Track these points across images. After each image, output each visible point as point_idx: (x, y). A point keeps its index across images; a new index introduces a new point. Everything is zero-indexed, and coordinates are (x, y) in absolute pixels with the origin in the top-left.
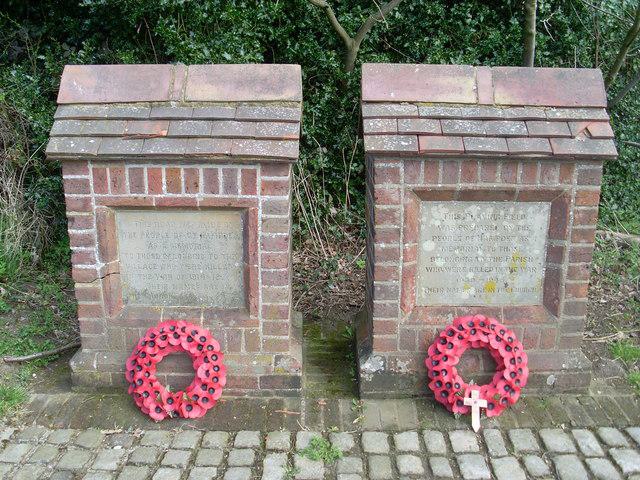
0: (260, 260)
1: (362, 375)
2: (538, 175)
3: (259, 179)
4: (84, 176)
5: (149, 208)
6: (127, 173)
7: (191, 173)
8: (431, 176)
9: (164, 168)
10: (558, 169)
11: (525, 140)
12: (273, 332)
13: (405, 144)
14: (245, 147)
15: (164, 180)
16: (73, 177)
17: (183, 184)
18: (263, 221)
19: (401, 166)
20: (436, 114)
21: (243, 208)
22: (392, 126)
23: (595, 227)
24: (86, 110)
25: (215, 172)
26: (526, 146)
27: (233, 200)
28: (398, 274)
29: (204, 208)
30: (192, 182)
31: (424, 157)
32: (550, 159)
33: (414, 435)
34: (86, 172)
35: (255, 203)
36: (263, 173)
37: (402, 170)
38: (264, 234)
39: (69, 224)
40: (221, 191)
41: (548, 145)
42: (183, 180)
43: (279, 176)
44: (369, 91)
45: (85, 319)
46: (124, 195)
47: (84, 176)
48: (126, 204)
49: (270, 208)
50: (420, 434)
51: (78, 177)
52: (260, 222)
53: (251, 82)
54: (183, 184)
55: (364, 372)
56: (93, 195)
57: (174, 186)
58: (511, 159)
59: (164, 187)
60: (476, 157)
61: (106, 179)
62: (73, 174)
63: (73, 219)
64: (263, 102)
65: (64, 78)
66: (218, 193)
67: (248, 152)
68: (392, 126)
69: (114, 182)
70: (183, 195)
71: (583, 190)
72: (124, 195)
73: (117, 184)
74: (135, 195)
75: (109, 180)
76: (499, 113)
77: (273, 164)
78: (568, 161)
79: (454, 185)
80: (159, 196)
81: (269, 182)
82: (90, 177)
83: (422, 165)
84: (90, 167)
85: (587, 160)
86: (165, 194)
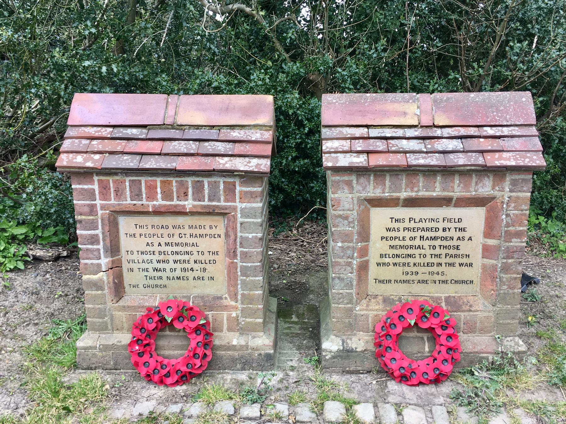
0: (239, 255)
1: (324, 354)
2: (473, 184)
3: (238, 188)
4: (90, 186)
5: (146, 213)
6: (127, 184)
7: (182, 185)
8: (467, 187)
9: (159, 180)
10: (491, 178)
11: (460, 155)
12: (250, 316)
13: (360, 160)
14: (226, 163)
15: (159, 190)
16: (81, 186)
17: (175, 194)
18: (241, 224)
19: (353, 178)
20: (383, 135)
21: (226, 214)
22: (346, 145)
23: (525, 228)
24: (92, 131)
25: (170, 183)
26: (461, 160)
27: (217, 207)
28: (352, 268)
29: (192, 213)
30: (183, 191)
31: (374, 171)
32: (484, 170)
33: (370, 406)
34: (92, 183)
35: (235, 209)
36: (242, 184)
37: (355, 182)
38: (242, 234)
39: (78, 225)
40: (206, 200)
41: (404, 158)
42: (175, 190)
43: (255, 187)
44: (327, 117)
45: (90, 306)
46: (125, 202)
47: (90, 186)
48: (127, 210)
49: (245, 213)
50: (375, 406)
51: (86, 187)
52: (239, 225)
53: (227, 110)
54: (175, 194)
55: (326, 350)
56: (98, 202)
57: (167, 196)
58: (448, 171)
59: (159, 196)
60: (419, 171)
61: (110, 189)
62: (79, 184)
63: (80, 222)
64: (242, 127)
65: (75, 105)
66: (204, 201)
67: (228, 166)
68: (346, 145)
69: (116, 191)
70: (175, 202)
71: (515, 199)
72: (125, 202)
73: (119, 193)
74: (135, 202)
75: (112, 190)
76: (438, 132)
77: (249, 177)
78: (499, 172)
79: (398, 194)
80: (155, 203)
81: (246, 192)
82: (96, 187)
83: (388, 178)
84: (96, 178)
85: (517, 171)
86: (160, 202)
